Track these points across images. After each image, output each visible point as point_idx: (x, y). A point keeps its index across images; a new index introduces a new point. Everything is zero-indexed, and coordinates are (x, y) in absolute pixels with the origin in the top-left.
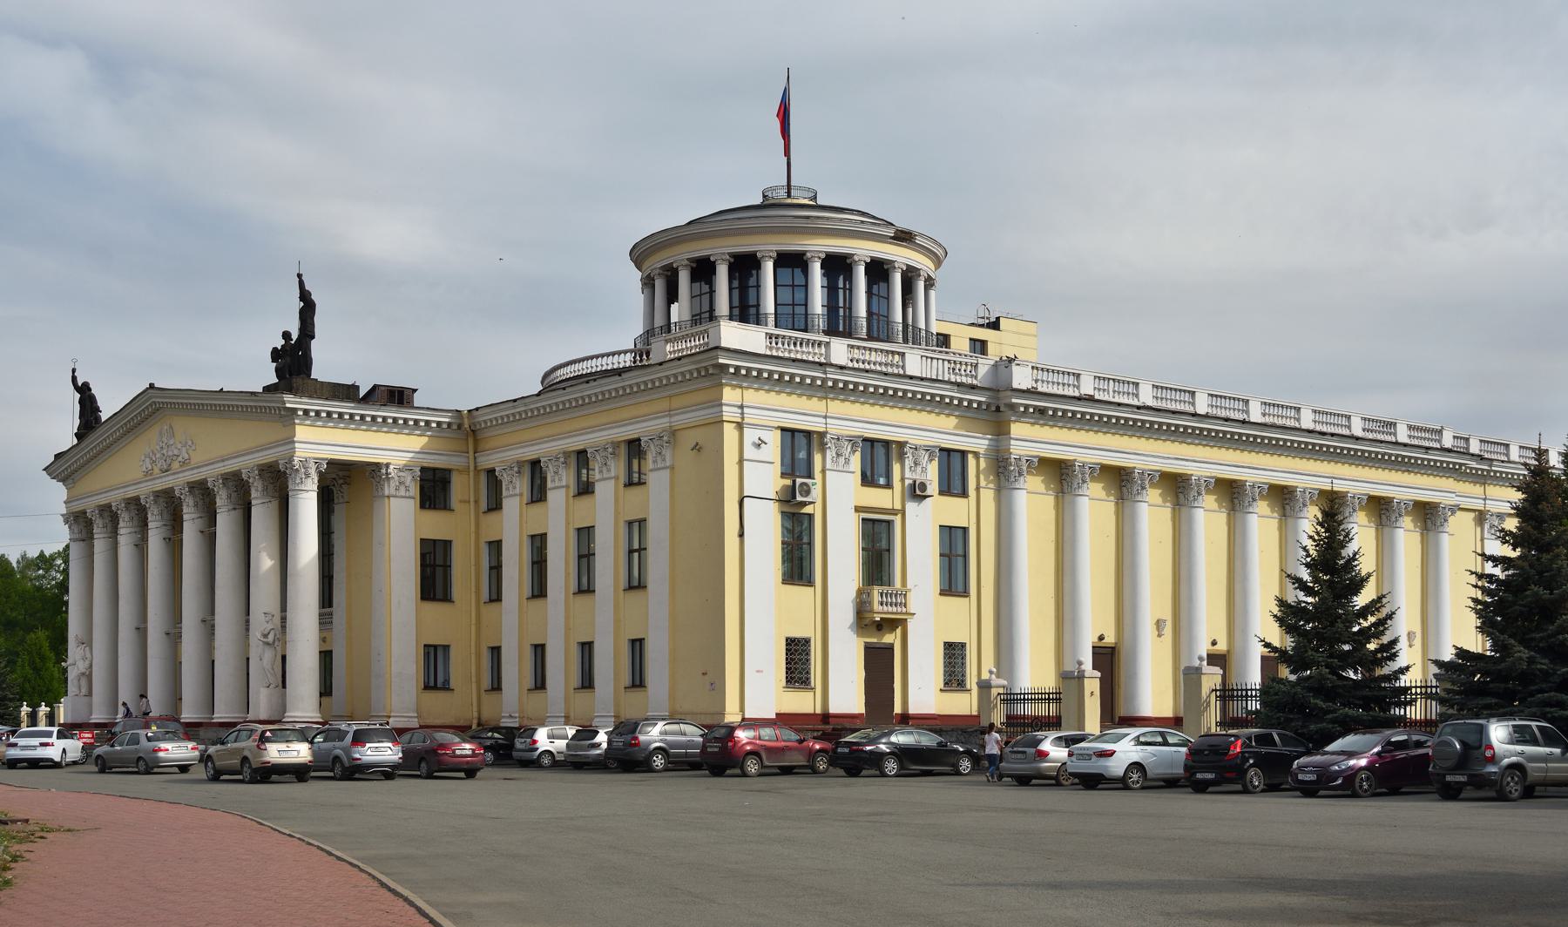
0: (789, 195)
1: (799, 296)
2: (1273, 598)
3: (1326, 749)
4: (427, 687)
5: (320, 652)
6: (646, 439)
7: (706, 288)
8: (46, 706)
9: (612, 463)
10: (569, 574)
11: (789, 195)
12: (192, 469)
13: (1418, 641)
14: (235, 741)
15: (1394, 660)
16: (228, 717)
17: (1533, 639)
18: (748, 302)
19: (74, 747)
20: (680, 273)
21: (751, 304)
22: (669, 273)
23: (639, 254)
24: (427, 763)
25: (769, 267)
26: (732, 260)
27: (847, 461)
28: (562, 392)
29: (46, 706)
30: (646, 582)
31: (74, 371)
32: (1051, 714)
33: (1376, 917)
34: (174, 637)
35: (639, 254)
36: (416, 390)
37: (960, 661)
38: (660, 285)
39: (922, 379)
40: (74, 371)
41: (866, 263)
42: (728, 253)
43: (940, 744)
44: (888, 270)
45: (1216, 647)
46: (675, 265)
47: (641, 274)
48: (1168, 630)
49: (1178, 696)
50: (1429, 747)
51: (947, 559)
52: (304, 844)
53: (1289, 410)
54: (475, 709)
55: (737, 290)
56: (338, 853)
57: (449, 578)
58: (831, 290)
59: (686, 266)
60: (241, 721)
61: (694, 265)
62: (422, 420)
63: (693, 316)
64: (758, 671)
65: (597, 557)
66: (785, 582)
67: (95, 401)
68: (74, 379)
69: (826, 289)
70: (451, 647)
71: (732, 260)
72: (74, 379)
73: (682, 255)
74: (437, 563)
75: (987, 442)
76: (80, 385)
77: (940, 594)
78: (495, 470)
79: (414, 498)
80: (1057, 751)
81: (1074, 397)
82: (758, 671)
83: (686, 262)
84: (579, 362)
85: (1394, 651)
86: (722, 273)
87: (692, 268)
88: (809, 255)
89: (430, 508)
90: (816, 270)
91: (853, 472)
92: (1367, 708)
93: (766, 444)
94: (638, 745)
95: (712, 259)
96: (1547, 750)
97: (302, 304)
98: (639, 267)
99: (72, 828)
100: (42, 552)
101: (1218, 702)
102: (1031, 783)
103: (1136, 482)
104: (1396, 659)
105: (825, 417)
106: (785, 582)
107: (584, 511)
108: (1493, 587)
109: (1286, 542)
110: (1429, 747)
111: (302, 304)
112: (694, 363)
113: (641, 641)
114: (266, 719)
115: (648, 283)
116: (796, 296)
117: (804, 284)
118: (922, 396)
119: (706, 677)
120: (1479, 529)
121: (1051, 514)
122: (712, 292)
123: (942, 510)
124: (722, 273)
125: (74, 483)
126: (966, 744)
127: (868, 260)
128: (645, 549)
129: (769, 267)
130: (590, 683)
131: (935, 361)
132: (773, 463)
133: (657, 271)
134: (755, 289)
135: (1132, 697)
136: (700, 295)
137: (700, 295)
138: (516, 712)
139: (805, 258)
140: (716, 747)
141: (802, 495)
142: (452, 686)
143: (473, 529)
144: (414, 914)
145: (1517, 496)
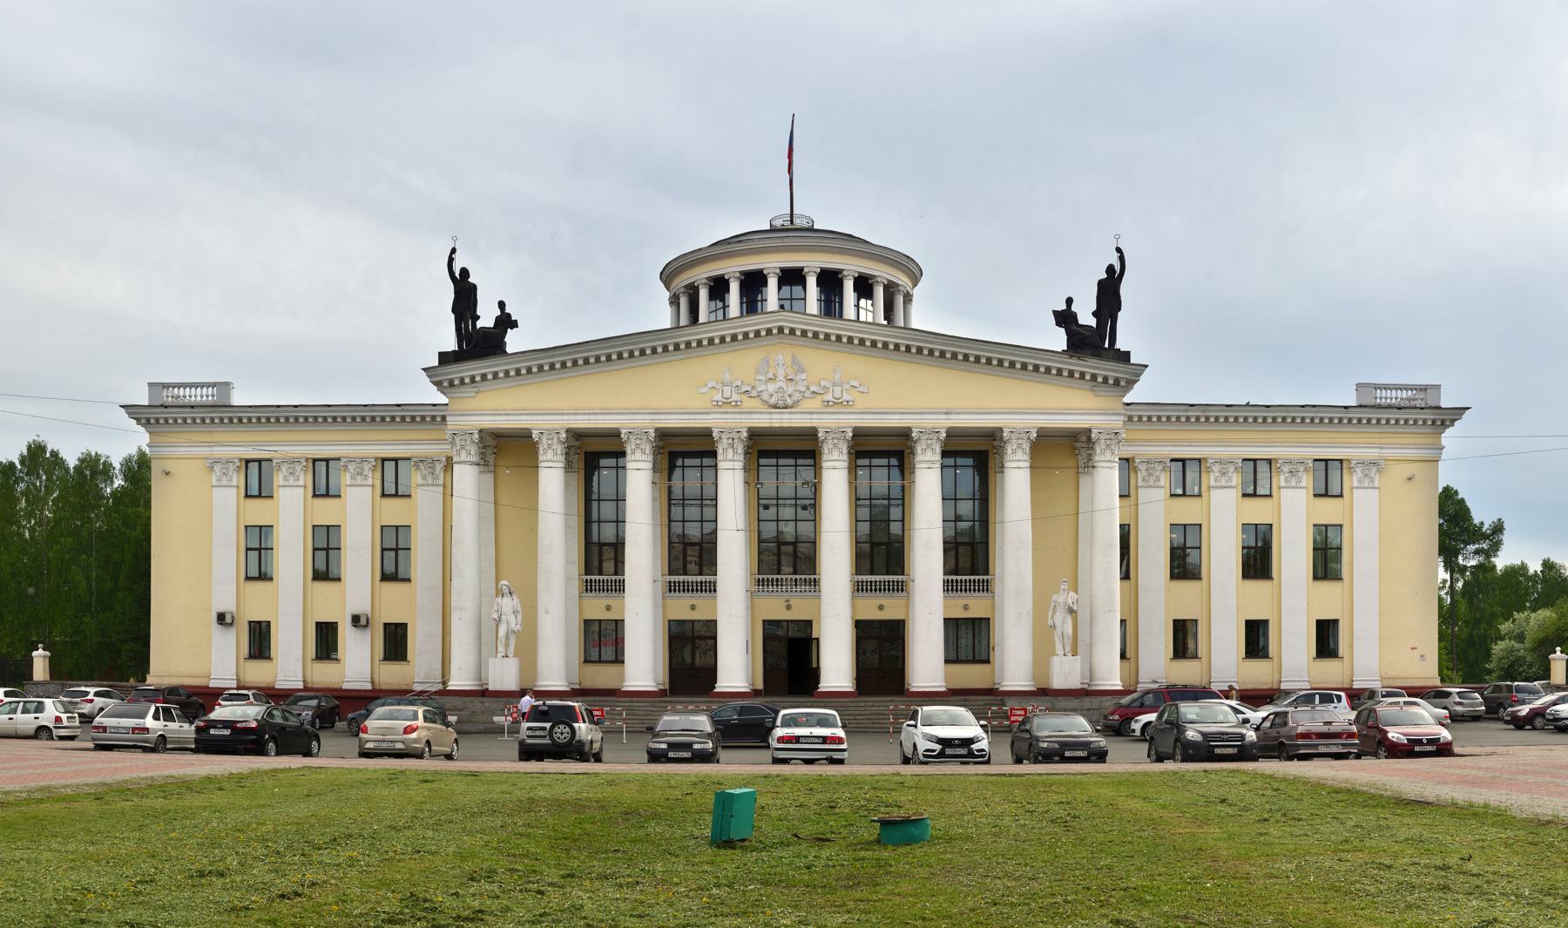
0: (792, 223)
1: (708, 512)
2: (233, 382)
3: (213, 716)
4: (586, 661)
5: (944, 619)
6: (416, 460)
7: (720, 305)
8: (1562, 652)
9: (1304, 477)
10: (1264, 635)
11: (792, 223)
12: (741, 413)
13: (699, 704)
16: (466, 685)
18: (705, 458)
20: (731, 284)
21: (593, 520)
22: (691, 292)
23: (668, 275)
25: (773, 283)
26: (743, 278)
27: (1158, 479)
28: (1378, 436)
29: (44, 649)
30: (624, 517)
31: (454, 251)
35: (668, 275)
37: (1176, 563)
38: (684, 301)
39: (1406, 408)
40: (454, 251)
41: (855, 278)
42: (740, 272)
44: (893, 292)
46: (696, 284)
47: (668, 293)
48: (1325, 729)
49: (210, 409)
53: (1378, 391)
54: (1011, 683)
55: (958, 459)
56: (1004, 778)
57: (1250, 693)
58: (671, 502)
59: (705, 284)
61: (712, 284)
62: (329, 416)
63: (1003, 472)
64: (1412, 649)
65: (628, 526)
67: (537, 761)
68: (451, 261)
69: (47, 660)
70: (1341, 623)
71: (743, 278)
72: (451, 261)
73: (701, 274)
74: (887, 464)
75: (1006, 683)
76: (478, 327)
78: (712, 432)
79: (1306, 488)
80: (522, 412)
82: (1412, 649)
83: (738, 274)
84: (174, 387)
86: (734, 288)
87: (710, 286)
88: (806, 270)
89: (260, 623)
90: (812, 282)
91: (1163, 487)
94: (494, 723)
95: (726, 277)
96: (732, 791)
97: (1105, 276)
98: (668, 288)
99: (448, 293)
100: (1055, 312)
101: (745, 305)
103: (1013, 909)
104: (93, 454)
105: (889, 499)
107: (1256, 599)
108: (912, 707)
109: (803, 440)
111: (1105, 276)
112: (1435, 414)
113: (252, 656)
114: (1079, 686)
115: (674, 301)
116: (875, 483)
117: (257, 464)
118: (1037, 759)
119: (1415, 651)
120: (792, 761)
121: (493, 480)
123: (340, 602)
124: (734, 288)
125: (477, 393)
126: (1142, 697)
127: (819, 270)
128: (766, 300)
129: (773, 283)
130: (321, 630)
133: (682, 290)
134: (700, 464)
135: (766, 308)
136: (716, 311)
137: (716, 311)
138: (190, 743)
139: (803, 273)
142: (1199, 656)
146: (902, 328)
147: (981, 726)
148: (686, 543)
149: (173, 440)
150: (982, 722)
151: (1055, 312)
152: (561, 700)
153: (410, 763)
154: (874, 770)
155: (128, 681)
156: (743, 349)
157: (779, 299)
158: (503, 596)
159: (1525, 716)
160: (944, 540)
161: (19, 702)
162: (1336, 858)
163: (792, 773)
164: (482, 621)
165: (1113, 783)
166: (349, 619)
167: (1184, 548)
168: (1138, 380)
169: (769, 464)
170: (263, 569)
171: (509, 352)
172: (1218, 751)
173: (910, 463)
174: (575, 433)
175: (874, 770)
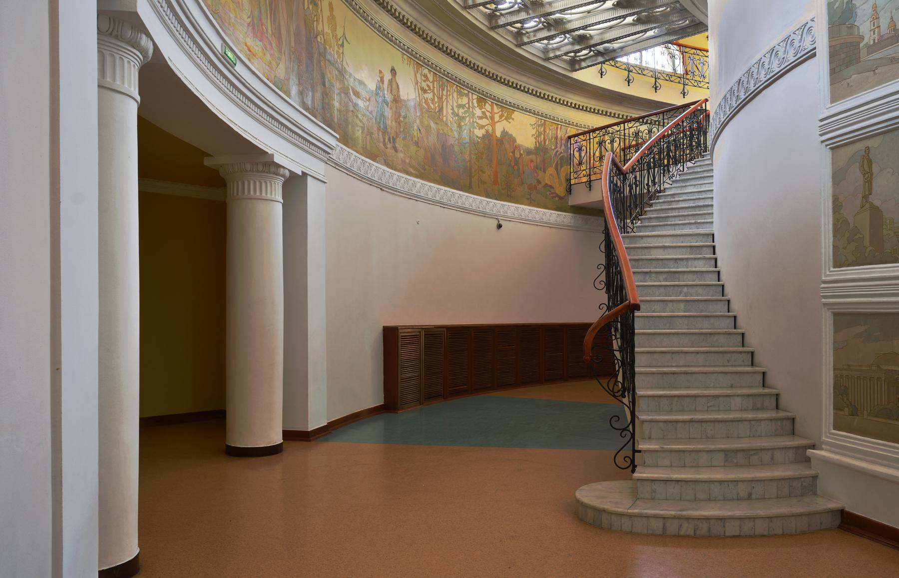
12: (110, 51)
14: (658, 132)
15: (397, 413)
17: (522, 5)
19: (341, 48)
24: (834, 8)
32: (638, 193)
33: (382, 127)
34: (857, 391)
36: (380, 70)
43: (521, 26)
45: (357, 132)
50: (458, 111)
51: (636, 449)
52: (206, 97)
60: (317, 50)
66: (383, 326)
77: (390, 335)
81: (698, 49)
85: (457, 148)
92: (667, 155)
93: (590, 190)
102: (509, 120)
106: (383, 326)
110: (458, 111)
122: (745, 366)
131: (559, 126)
132: (325, 183)
140: (657, 12)
141: (825, 438)
143: (859, 98)
144: (654, 54)
145: (461, 109)
169: (660, 239)
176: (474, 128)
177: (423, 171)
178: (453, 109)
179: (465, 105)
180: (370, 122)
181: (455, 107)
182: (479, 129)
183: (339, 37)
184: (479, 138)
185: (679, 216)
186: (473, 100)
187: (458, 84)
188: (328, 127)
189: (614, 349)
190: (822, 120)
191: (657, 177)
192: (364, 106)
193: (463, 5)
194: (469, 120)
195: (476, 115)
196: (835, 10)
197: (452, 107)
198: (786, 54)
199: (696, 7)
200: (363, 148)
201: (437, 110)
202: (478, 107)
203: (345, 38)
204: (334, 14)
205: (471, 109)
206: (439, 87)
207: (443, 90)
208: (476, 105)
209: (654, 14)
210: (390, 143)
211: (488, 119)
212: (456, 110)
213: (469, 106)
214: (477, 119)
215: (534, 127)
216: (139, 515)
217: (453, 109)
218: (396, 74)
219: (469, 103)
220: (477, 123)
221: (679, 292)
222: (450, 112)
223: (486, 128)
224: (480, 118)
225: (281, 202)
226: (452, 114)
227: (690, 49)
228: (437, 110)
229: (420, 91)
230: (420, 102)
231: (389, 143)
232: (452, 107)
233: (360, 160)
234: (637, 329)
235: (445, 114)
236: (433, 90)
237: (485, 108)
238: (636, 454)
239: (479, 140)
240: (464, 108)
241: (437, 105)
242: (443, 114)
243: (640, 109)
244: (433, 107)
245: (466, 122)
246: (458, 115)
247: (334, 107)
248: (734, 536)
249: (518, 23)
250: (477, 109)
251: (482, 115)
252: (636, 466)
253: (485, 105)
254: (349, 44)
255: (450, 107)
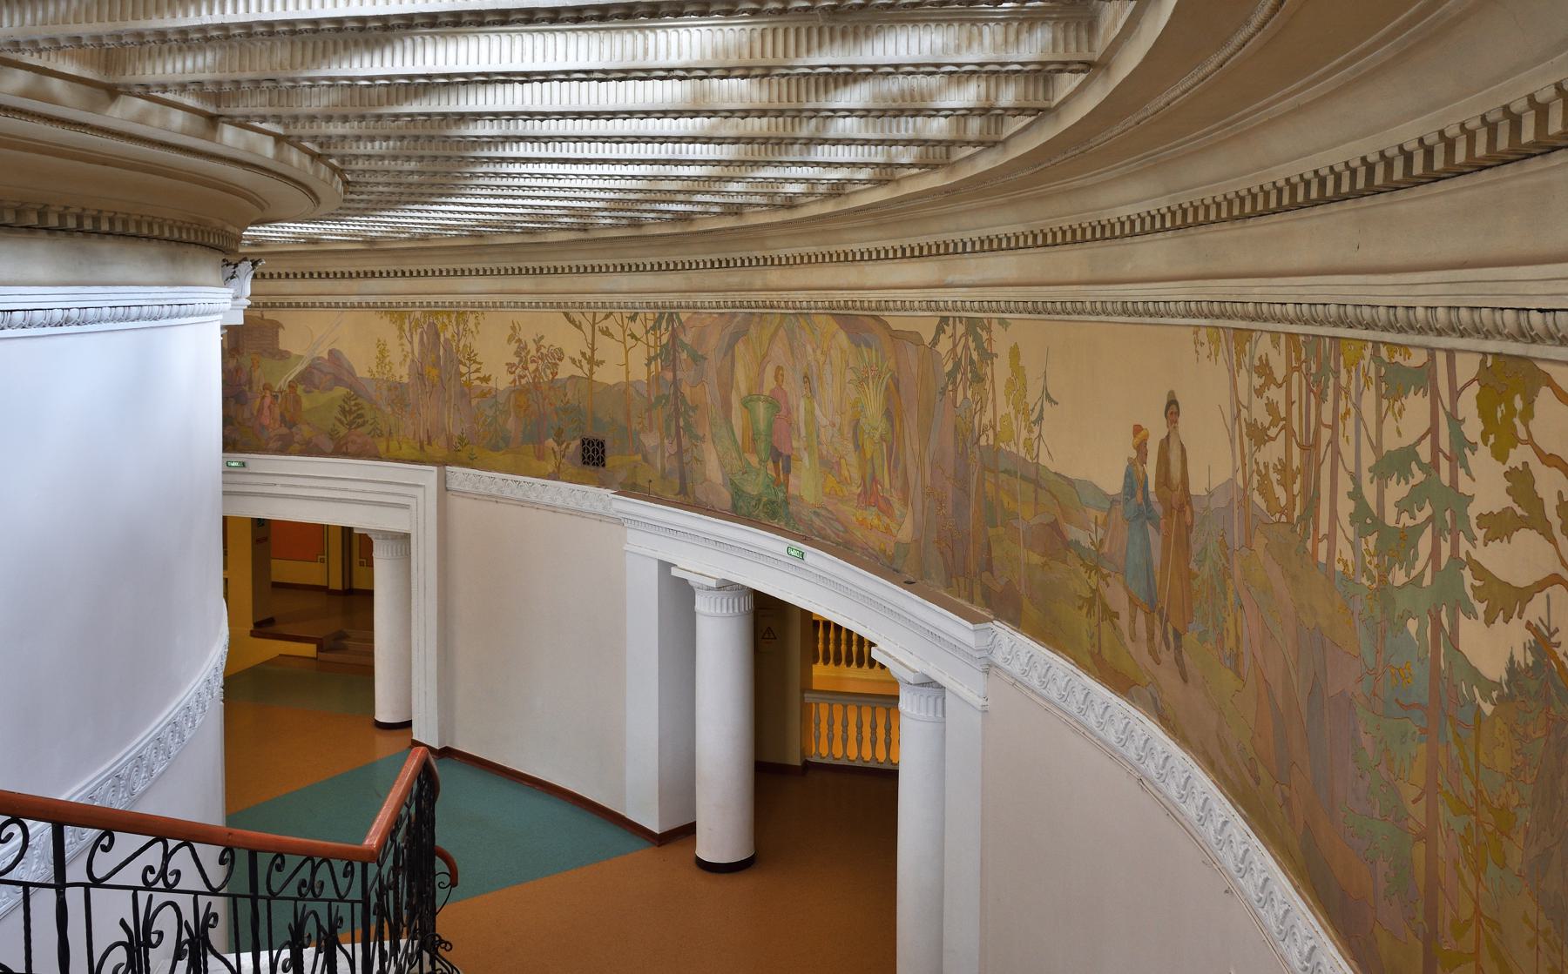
2: (1131, 446)
146: (1102, 745)
147: (279, 359)
148: (186, 86)
149: (182, 696)
150: (277, 357)
151: (283, 328)
152: (327, 846)
153: (1270, 863)
154: (1342, 58)
155: (1255, 445)
156: (116, 156)
157: (223, 483)
158: (741, 97)
159: (1513, 398)
160: (695, 833)
161: (665, 313)
162: (344, 909)
163: (312, 358)
164: (699, 572)
165: (592, 361)
166: (1229, 833)
167: (238, 369)
168: (1148, 435)
169: (291, 478)
170: (939, 701)
171: (1425, 352)
172: (340, 957)
173: (356, 44)
174: (69, 37)
175: (1342, 58)
176: (1461, 606)
177: (1251, 781)
178: (1356, 495)
179: (1410, 453)
180: (1545, 830)
181: (1366, 476)
182: (1489, 621)
183: (1030, 407)
184: (1487, 686)
185: (848, 583)
186: (1455, 394)
187: (802, 311)
188: (1397, 17)
189: (361, 904)
190: (406, 507)
191: (961, 387)
192: (1093, 543)
193: (1448, 454)
194: (1435, 554)
195: (1473, 511)
196: (1489, 528)
197: (1355, 478)
198: (264, 204)
199: (350, 491)
200: (1092, 655)
201: (1297, 513)
202: (1484, 437)
203: (1048, 395)
204: (1549, 388)
205: (1444, 465)
206: (1310, 390)
207: (1321, 399)
208: (1473, 428)
209: (413, 825)
210: (1168, 648)
211: (1546, 531)
212: (1370, 492)
213: (1436, 449)
214: (1480, 534)
215: (372, 434)
216: (896, 883)
217: (1356, 495)
218: (1178, 413)
219: (1433, 430)
220: (1479, 570)
221: (394, 435)
222: (1346, 507)
223: (1535, 609)
224: (1499, 526)
225: (1528, 317)
226: (1354, 519)
227: (591, 321)
228: (1297, 513)
229: (1246, 439)
230: (1245, 490)
231: (1164, 647)
232: (1355, 478)
233: (1267, 337)
234: (915, 123)
235: (1324, 528)
236: (1288, 418)
237: (1530, 441)
238: (349, 904)
239: (1488, 708)
240: (1405, 474)
241: (1297, 488)
242: (1316, 529)
243: (865, 227)
244: (1283, 502)
245: (1419, 565)
246: (1378, 524)
247: (409, 366)
248: (943, 834)
249: (380, 967)
250: (1482, 460)
251: (1508, 501)
252: (541, 83)
253: (1528, 414)
254: (1474, 480)
255: (1345, 485)
